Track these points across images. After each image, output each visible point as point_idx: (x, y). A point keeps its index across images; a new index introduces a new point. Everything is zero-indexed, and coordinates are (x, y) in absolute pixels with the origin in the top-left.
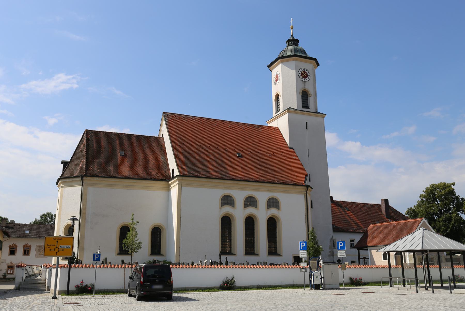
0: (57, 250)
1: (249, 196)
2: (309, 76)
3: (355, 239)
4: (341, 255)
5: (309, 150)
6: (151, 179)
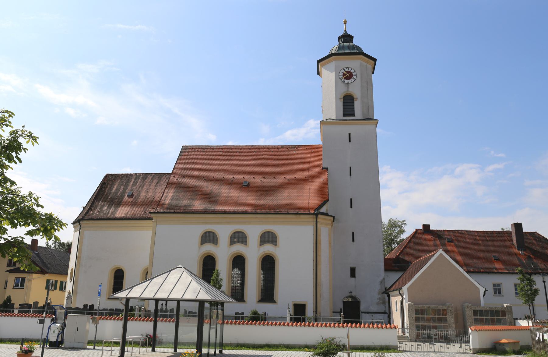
1: (267, 232)
2: (355, 75)
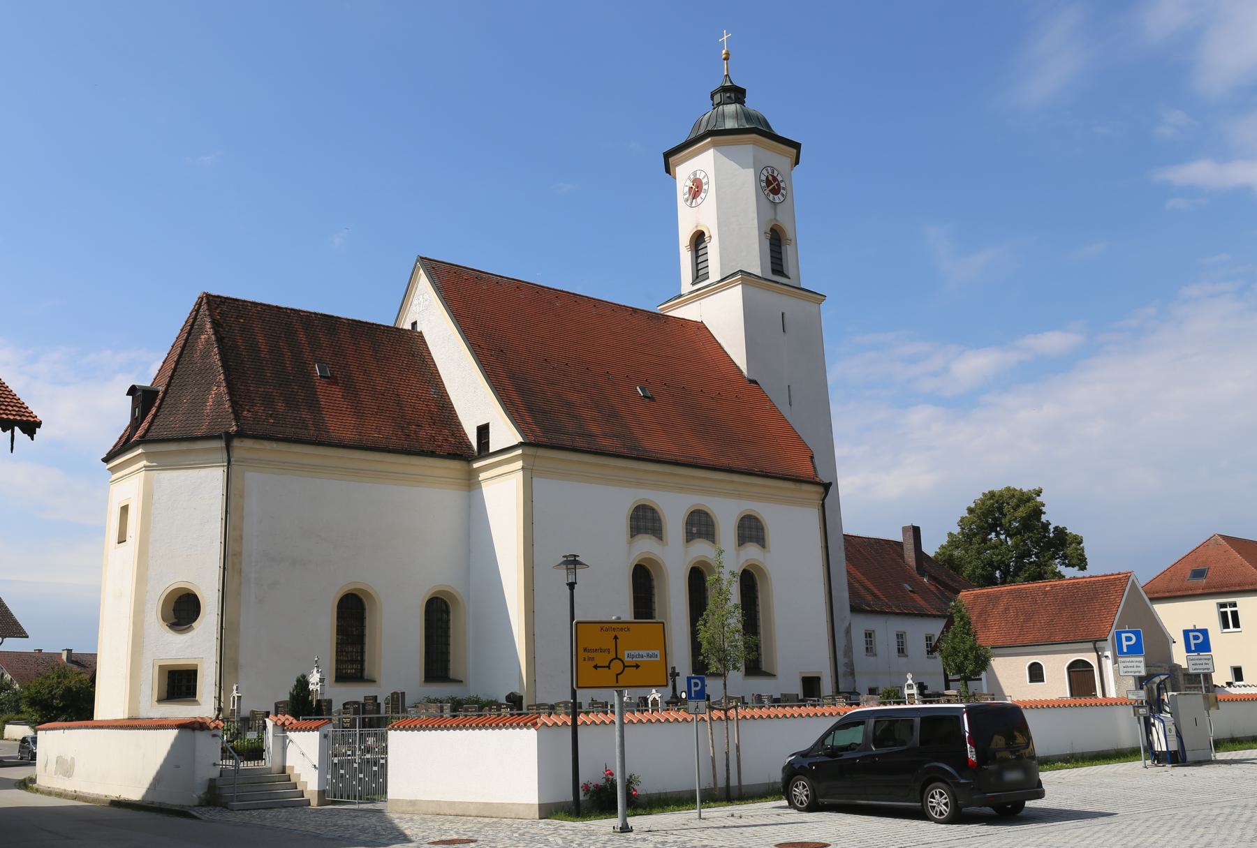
0: (617, 666)
2: (784, 189)
3: (874, 631)
4: (1129, 669)
5: (791, 387)
6: (423, 451)
